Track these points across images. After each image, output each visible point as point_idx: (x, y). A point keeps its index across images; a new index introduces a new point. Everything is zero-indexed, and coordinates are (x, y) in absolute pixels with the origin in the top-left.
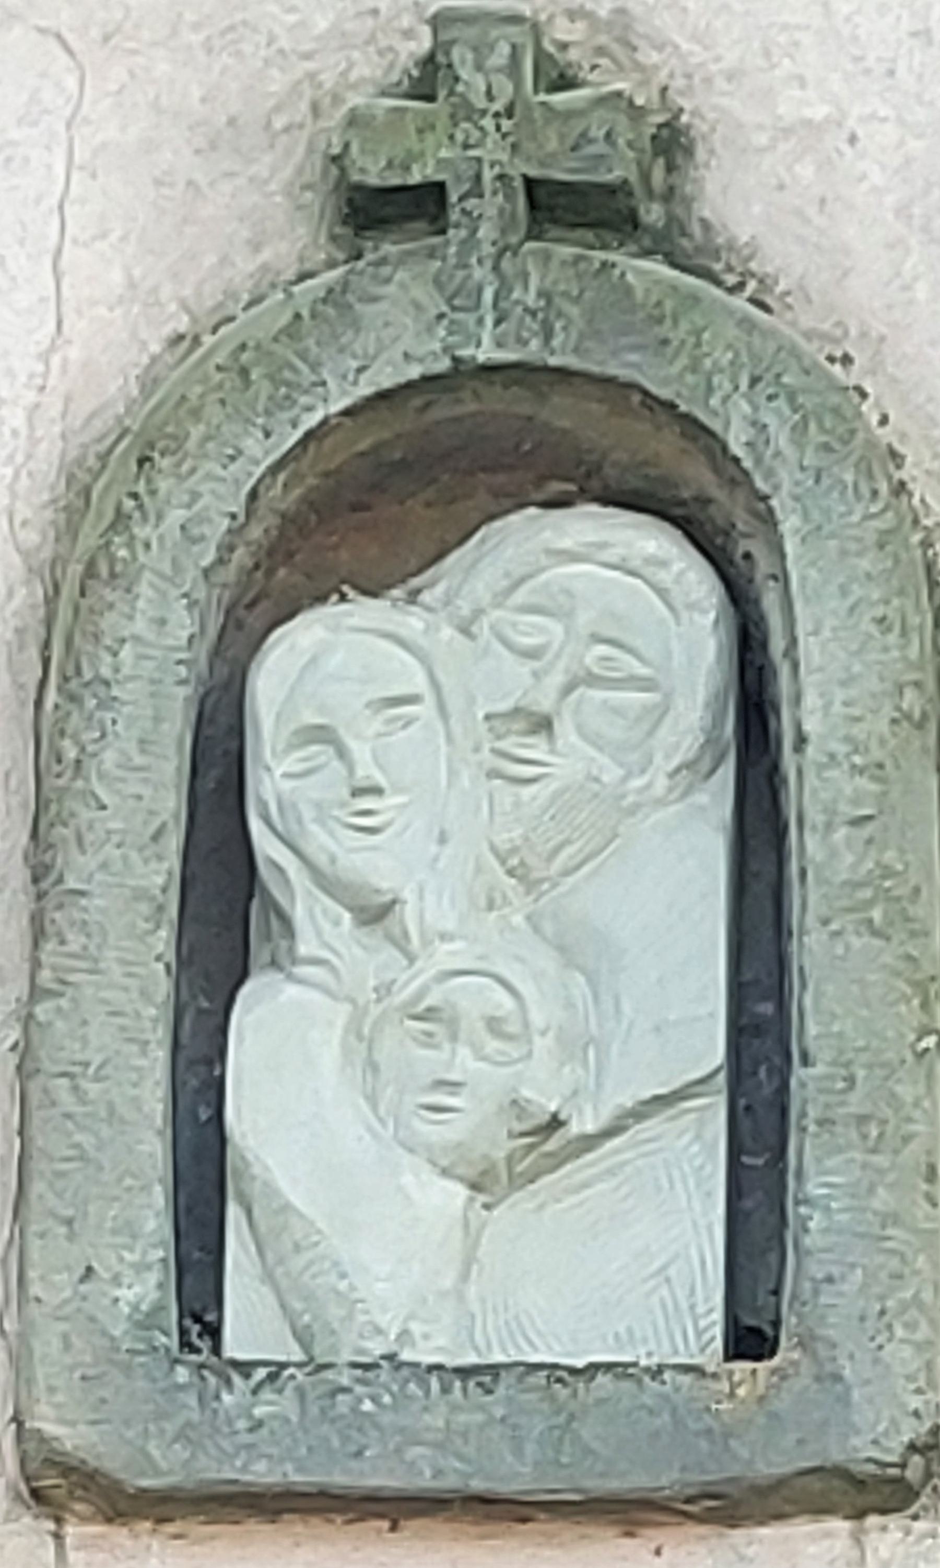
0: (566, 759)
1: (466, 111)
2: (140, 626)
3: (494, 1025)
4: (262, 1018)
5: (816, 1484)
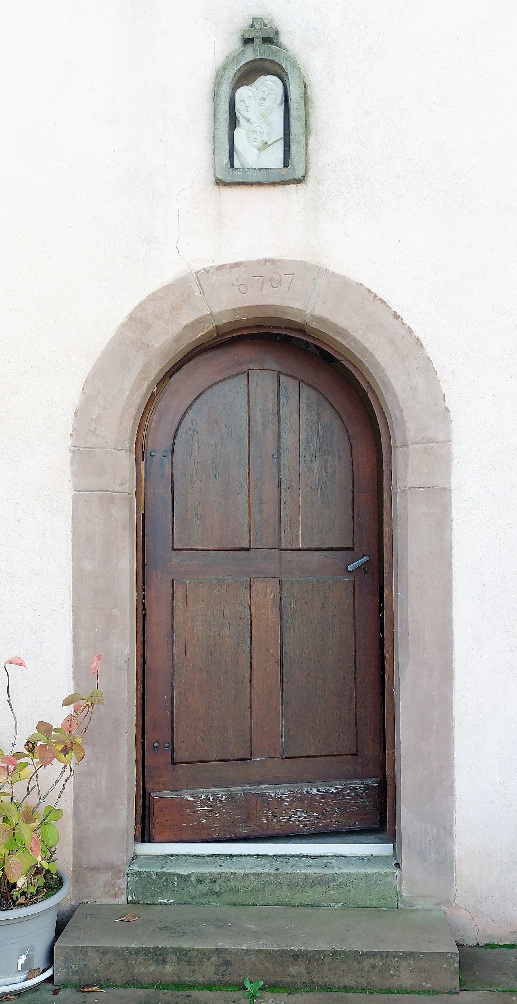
0: (267, 103)
1: (255, 29)
2: (224, 89)
3: (260, 132)
4: (237, 132)
5: (292, 181)
